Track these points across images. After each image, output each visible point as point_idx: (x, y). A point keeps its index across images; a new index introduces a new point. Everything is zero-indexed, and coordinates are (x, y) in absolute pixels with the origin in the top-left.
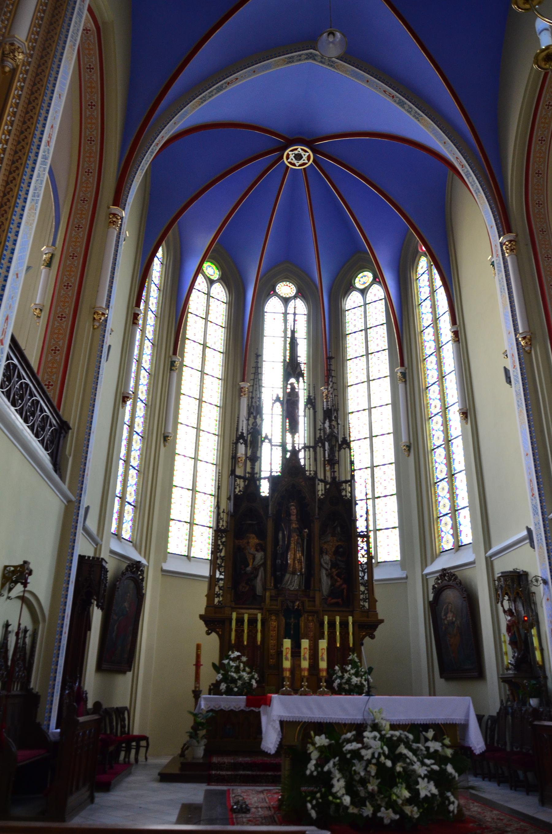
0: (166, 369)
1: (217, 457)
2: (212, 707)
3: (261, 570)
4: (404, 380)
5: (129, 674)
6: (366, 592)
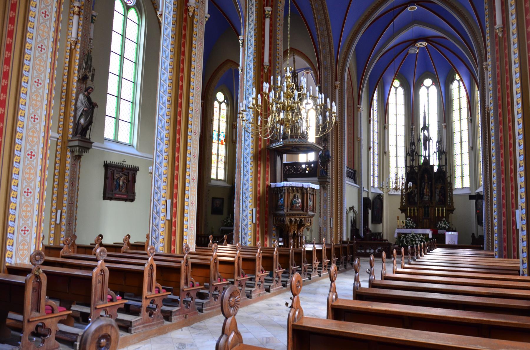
5: (381, 224)
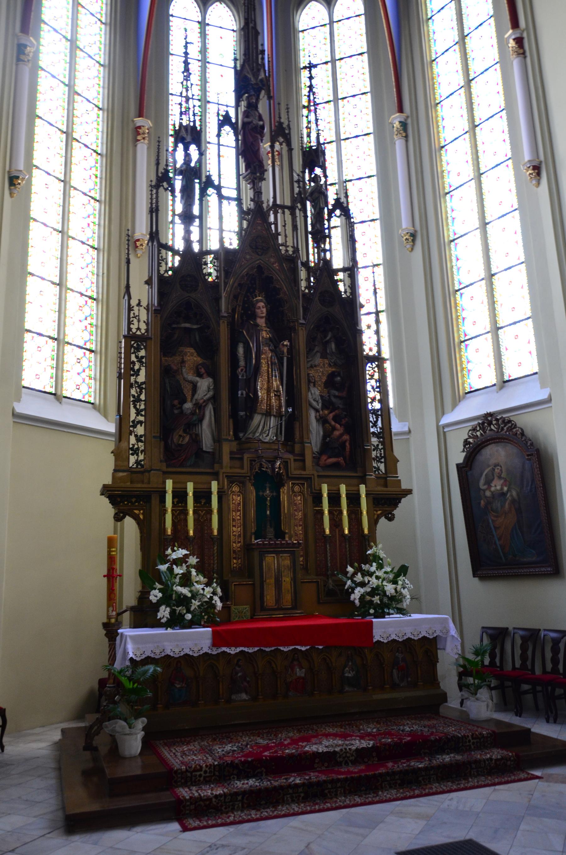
0: (9, 59)
1: (99, 237)
2: (148, 654)
3: (209, 412)
4: (404, 134)
6: (380, 447)
